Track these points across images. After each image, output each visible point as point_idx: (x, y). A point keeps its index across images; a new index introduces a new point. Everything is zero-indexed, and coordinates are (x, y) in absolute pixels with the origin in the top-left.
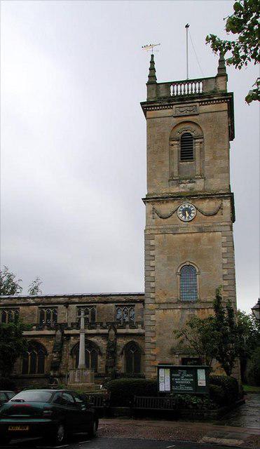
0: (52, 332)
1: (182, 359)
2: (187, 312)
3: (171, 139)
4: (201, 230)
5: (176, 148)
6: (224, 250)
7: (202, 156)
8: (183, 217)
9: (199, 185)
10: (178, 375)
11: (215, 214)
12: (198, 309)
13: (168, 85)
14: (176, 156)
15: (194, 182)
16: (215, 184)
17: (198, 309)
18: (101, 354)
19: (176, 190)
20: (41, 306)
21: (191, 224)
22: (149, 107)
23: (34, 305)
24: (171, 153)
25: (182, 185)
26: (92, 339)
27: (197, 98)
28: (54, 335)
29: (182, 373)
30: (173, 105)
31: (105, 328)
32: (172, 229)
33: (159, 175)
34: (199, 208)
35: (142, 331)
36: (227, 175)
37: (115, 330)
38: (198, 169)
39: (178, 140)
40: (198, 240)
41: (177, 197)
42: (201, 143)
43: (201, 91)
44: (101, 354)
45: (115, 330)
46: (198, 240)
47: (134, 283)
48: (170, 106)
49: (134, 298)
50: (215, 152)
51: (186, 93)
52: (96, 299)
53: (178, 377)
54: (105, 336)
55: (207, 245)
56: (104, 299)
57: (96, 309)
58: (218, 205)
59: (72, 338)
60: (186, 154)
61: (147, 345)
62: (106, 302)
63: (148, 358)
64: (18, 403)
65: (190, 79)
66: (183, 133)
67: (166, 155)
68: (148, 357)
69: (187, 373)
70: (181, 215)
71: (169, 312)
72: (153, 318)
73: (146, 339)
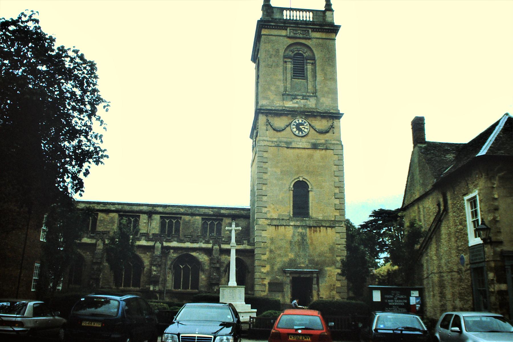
0: (151, 244)
1: (293, 278)
2: (300, 230)
3: (285, 57)
4: (315, 147)
5: (289, 66)
6: (335, 168)
7: (315, 76)
8: (297, 132)
9: (311, 103)
10: (391, 297)
11: (327, 132)
12: (310, 227)
13: (282, 9)
14: (289, 76)
15: (307, 99)
16: (325, 103)
17: (310, 227)
18: (203, 271)
19: (289, 104)
20: (122, 213)
21: (304, 140)
22: (266, 25)
23: (113, 211)
24: (285, 69)
25: (295, 101)
26: (194, 254)
27: (310, 24)
28: (153, 248)
29: (395, 294)
30: (287, 27)
31: (207, 242)
32: (286, 143)
33: (273, 88)
34: (312, 124)
35: (248, 247)
36: (263, 102)
37: (220, 246)
38: (310, 87)
39: (291, 58)
40: (311, 157)
41: (293, 113)
42: (312, 64)
43: (311, 20)
44: (203, 271)
45: (220, 246)
46: (311, 157)
47: (236, 195)
48: (285, 28)
49: (222, 211)
50: (325, 74)
51: (292, 18)
52: (182, 210)
53: (390, 299)
54: (208, 252)
55: (320, 162)
56: (190, 211)
57: (181, 222)
58: (330, 123)
59: (172, 251)
60: (299, 72)
61: (257, 263)
62: (193, 215)
63: (258, 277)
64: (289, 330)
65: (292, 7)
66: (295, 52)
67: (280, 69)
68: (257, 275)
69: (401, 294)
70: (295, 130)
71: (282, 229)
72: (264, 234)
73: (256, 257)
